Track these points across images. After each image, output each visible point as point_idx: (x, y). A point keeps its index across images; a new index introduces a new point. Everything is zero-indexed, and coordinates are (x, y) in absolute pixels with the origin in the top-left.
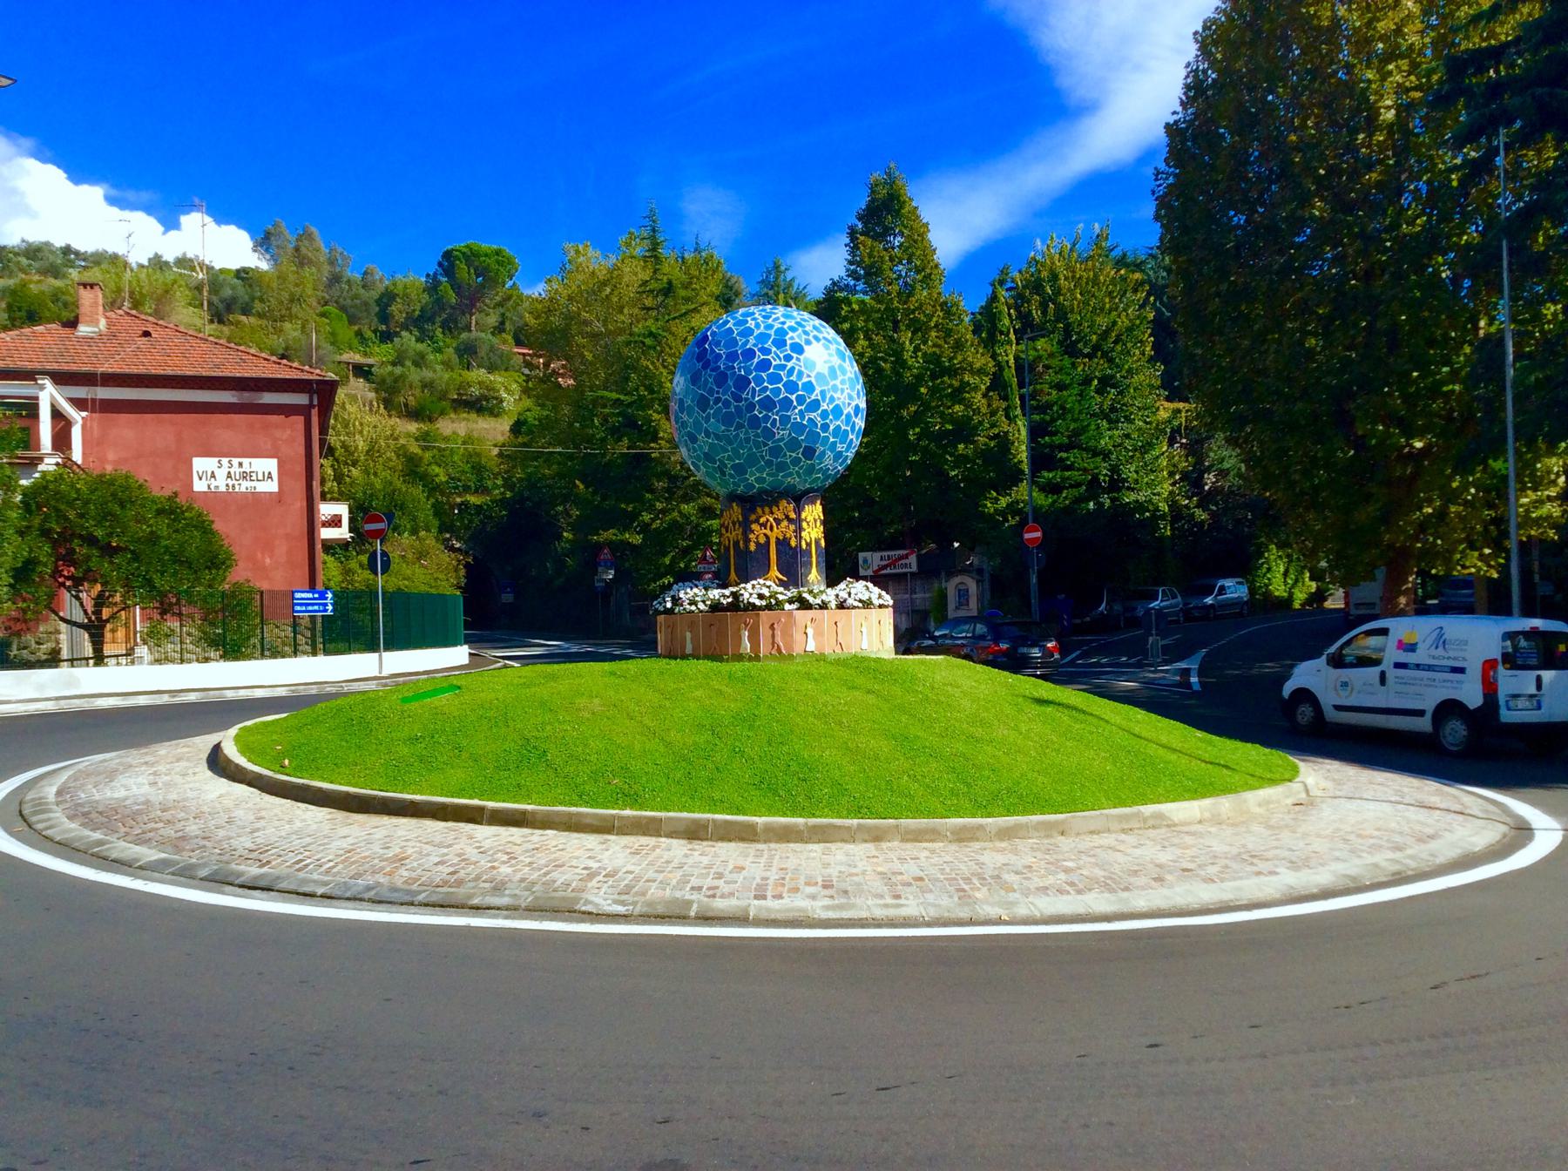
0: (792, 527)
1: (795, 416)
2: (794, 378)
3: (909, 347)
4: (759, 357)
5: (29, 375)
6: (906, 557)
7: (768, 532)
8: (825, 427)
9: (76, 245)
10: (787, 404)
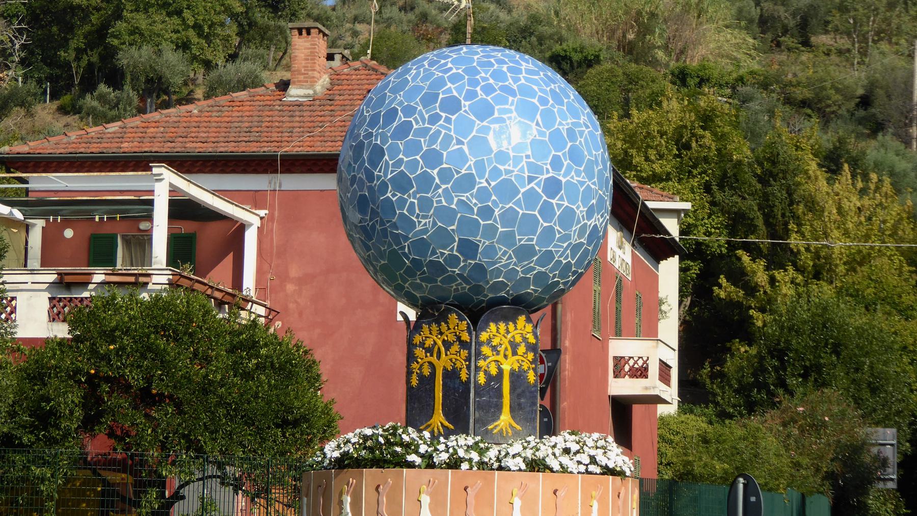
0: (464, 353)
1: (439, 198)
3: (95, 103)
4: (401, 117)
5: (140, 163)
7: (434, 359)
8: (486, 212)
10: (426, 181)
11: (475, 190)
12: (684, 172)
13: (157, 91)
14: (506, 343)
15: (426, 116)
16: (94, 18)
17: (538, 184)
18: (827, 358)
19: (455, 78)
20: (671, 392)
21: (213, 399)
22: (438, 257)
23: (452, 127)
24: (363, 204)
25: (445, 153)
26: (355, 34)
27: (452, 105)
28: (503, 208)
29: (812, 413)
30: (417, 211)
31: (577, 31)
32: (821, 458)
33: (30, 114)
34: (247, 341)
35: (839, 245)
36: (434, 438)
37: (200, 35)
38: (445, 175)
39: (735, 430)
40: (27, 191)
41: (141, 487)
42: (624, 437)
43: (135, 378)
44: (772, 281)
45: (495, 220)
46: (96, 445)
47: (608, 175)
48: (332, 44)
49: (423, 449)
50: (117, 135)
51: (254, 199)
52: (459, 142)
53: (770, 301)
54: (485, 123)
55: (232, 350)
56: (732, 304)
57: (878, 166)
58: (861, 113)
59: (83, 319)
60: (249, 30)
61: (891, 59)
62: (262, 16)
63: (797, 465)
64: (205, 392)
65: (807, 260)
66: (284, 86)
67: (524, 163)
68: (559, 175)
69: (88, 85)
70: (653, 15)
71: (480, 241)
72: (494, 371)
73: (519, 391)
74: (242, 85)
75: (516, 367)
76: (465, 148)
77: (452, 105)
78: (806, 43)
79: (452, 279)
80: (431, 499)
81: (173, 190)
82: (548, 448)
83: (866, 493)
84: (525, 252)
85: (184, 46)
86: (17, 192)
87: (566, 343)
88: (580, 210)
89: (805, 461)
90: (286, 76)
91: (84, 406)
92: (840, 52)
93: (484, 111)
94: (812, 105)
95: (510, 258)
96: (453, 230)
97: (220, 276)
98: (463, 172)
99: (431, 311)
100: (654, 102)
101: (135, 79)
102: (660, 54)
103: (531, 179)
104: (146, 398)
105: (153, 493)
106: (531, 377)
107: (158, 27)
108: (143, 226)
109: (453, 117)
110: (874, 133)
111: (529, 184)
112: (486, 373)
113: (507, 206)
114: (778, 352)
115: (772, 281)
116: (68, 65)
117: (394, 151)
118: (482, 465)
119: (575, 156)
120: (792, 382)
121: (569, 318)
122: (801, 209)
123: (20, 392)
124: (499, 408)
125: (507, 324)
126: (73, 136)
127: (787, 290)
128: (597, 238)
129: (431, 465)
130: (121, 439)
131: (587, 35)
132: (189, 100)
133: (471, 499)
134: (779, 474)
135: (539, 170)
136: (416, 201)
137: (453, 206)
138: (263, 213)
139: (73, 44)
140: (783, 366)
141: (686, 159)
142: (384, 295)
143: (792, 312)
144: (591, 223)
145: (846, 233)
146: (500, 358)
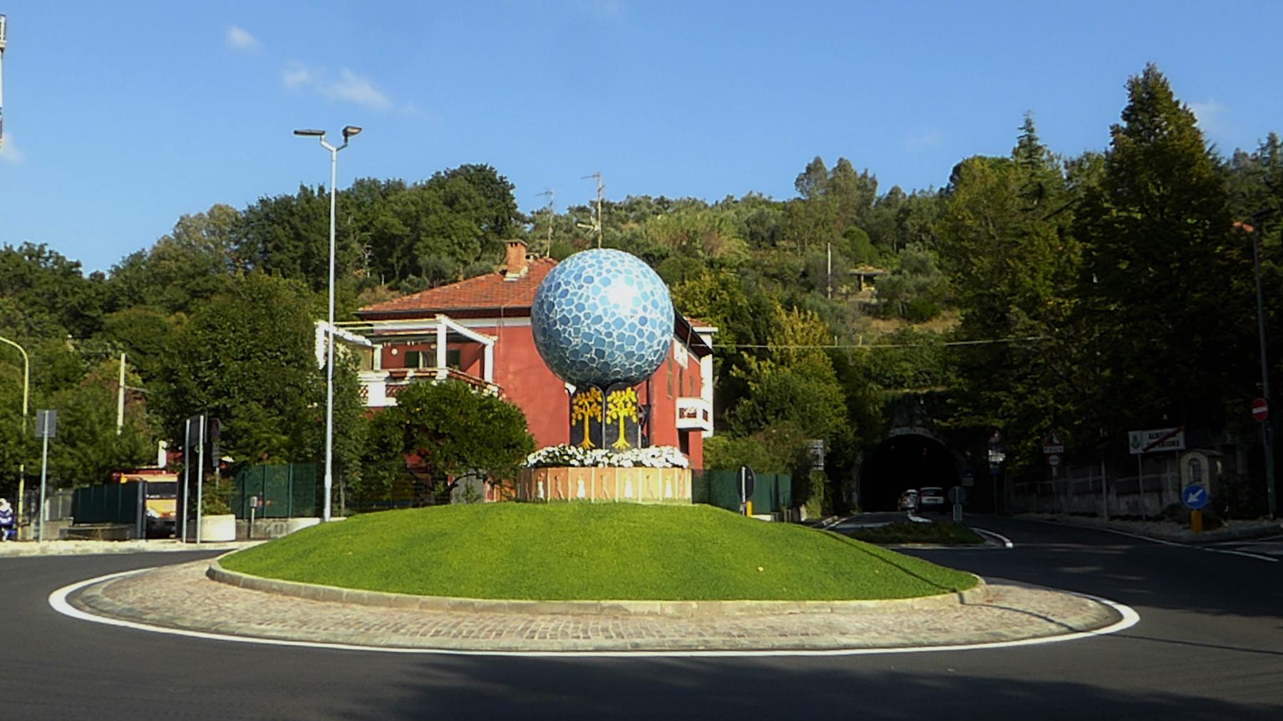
2: (582, 301)
4: (563, 287)
5: (430, 314)
6: (1173, 435)
8: (609, 335)
9: (667, 197)
12: (713, 313)
13: (439, 277)
16: (406, 241)
18: (787, 405)
19: (591, 266)
20: (709, 425)
21: (471, 435)
24: (544, 332)
26: (541, 245)
27: (590, 280)
29: (780, 433)
31: (656, 242)
32: (786, 455)
33: (374, 291)
34: (488, 405)
35: (793, 348)
36: (585, 453)
37: (461, 247)
38: (587, 316)
39: (741, 444)
40: (372, 331)
41: (435, 481)
42: (685, 449)
43: (430, 425)
44: (759, 366)
46: (412, 460)
47: (673, 314)
48: (529, 251)
49: (579, 457)
50: (417, 300)
51: (490, 332)
53: (758, 377)
55: (479, 410)
56: (738, 379)
57: (812, 308)
58: (802, 280)
59: (400, 394)
60: (486, 245)
61: (817, 253)
62: (492, 238)
63: (773, 460)
64: (467, 431)
65: (777, 356)
66: (504, 273)
69: (404, 275)
70: (695, 232)
74: (483, 273)
77: (590, 280)
78: (774, 245)
79: (592, 369)
81: (448, 328)
82: (644, 455)
83: (808, 473)
85: (453, 254)
86: (367, 331)
87: (654, 401)
88: (658, 332)
89: (777, 458)
90: (505, 267)
91: (405, 440)
92: (791, 250)
93: (607, 282)
94: (778, 277)
97: (473, 372)
99: (583, 387)
100: (697, 276)
101: (427, 271)
102: (700, 252)
104: (436, 436)
105: (442, 483)
106: (635, 419)
107: (439, 245)
108: (433, 347)
110: (809, 291)
114: (762, 403)
115: (759, 366)
116: (392, 265)
117: (560, 304)
118: (609, 464)
119: (655, 305)
120: (769, 418)
121: (655, 388)
122: (773, 330)
123: (371, 434)
126: (395, 301)
127: (767, 372)
128: (668, 347)
129: (583, 465)
130: (423, 457)
131: (662, 243)
132: (456, 281)
133: (605, 483)
134: (764, 464)
135: (636, 312)
138: (495, 338)
139: (395, 255)
140: (765, 410)
141: (714, 308)
142: (559, 379)
143: (769, 382)
144: (663, 339)
145: (796, 342)
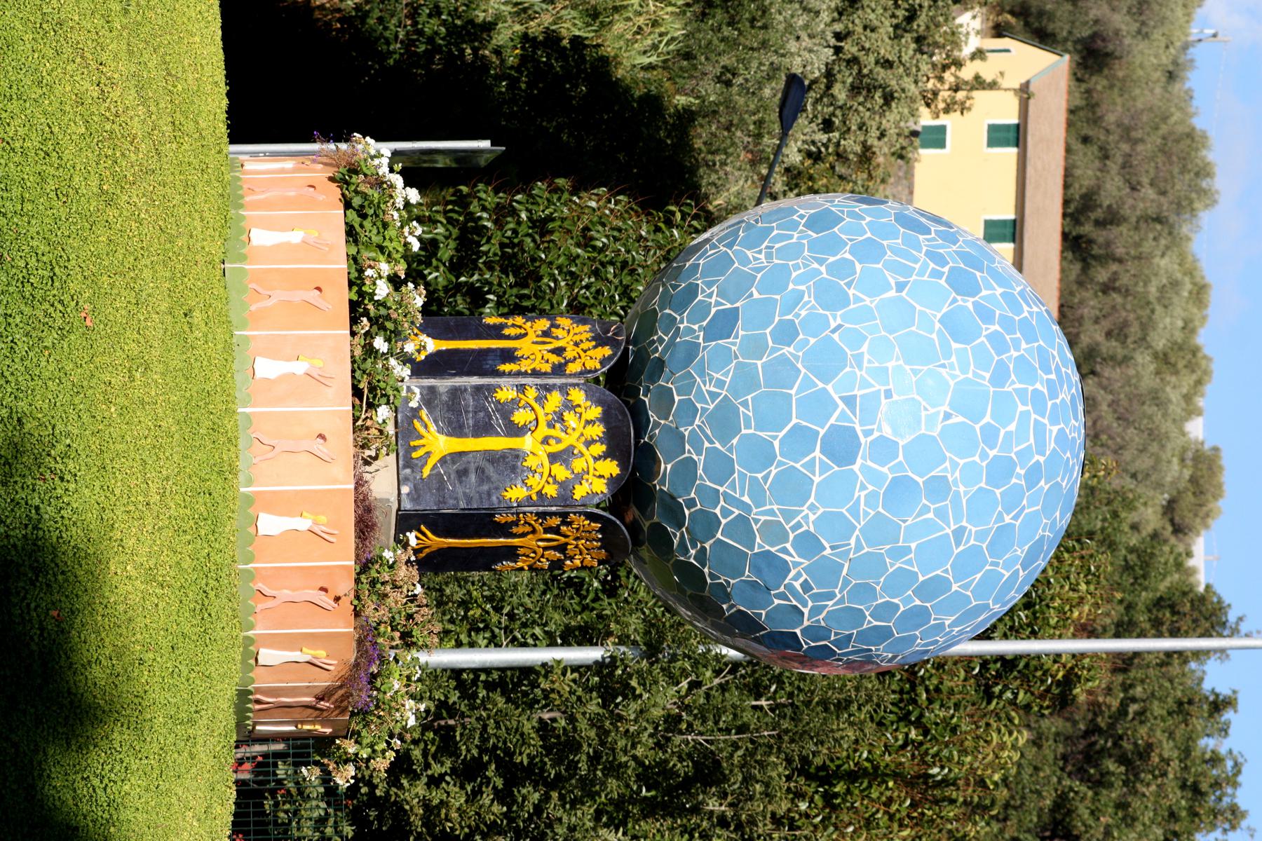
8: (787, 333)
11: (821, 311)
14: (568, 440)
15: (972, 542)
17: (843, 416)
22: (703, 291)
23: (925, 278)
25: (880, 266)
28: (797, 358)
30: (777, 246)
45: (774, 350)
52: (900, 287)
54: (938, 325)
67: (878, 387)
68: (864, 458)
71: (736, 337)
72: (520, 417)
73: (490, 470)
75: (531, 462)
76: (892, 293)
80: (296, 246)
84: (725, 421)
95: (714, 396)
96: (751, 295)
98: (851, 292)
103: (850, 401)
109: (942, 282)
111: (841, 398)
112: (515, 403)
113: (799, 366)
124: (456, 430)
125: (601, 441)
136: (794, 240)
137: (791, 286)
146: (543, 430)
